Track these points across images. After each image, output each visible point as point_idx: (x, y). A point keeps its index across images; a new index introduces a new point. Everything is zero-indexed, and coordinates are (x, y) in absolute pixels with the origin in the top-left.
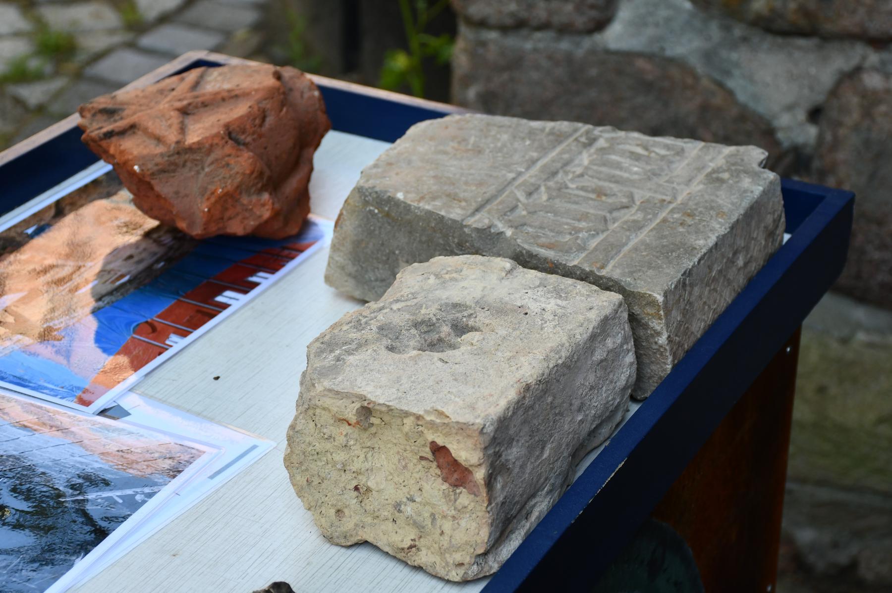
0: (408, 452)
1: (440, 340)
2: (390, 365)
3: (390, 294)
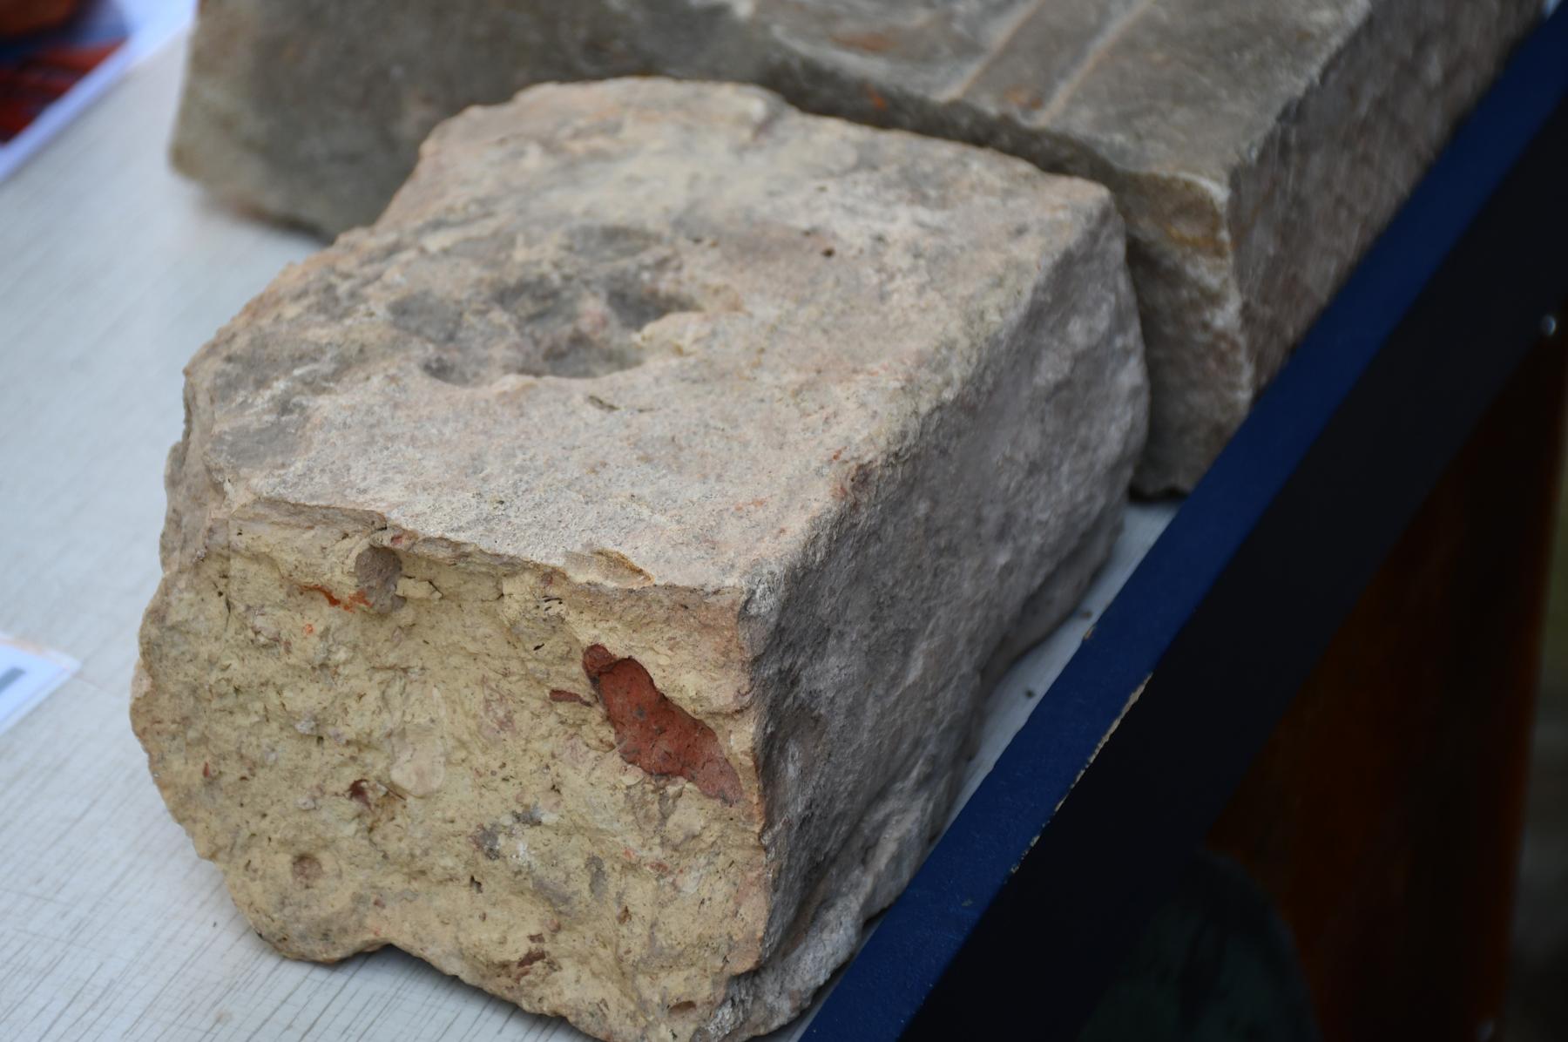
0: (514, 678)
1: (579, 340)
2: (446, 421)
3: (405, 208)
